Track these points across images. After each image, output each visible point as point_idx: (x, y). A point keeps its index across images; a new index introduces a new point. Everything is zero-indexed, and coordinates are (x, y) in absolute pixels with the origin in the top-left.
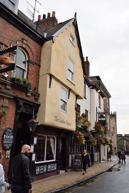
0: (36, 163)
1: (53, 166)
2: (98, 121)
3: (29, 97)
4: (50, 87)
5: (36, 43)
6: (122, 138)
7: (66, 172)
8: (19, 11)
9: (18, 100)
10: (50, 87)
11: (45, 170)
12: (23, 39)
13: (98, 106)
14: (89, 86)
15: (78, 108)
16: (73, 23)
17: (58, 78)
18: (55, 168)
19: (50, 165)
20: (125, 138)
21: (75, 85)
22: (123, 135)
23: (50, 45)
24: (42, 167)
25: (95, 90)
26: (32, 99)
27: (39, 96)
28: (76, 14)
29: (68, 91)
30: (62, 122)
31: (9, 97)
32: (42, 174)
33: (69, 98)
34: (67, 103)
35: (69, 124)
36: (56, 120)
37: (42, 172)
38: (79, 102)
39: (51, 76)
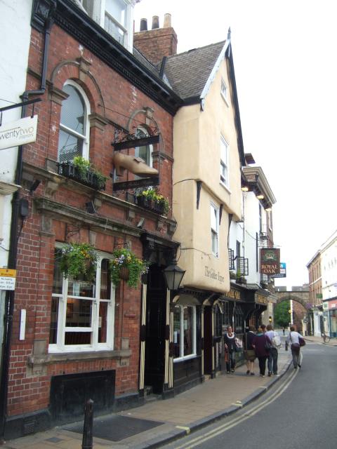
3: (131, 220)
4: (197, 208)
5: (165, 112)
6: (285, 295)
7: (212, 378)
9: (148, 239)
10: (197, 208)
12: (146, 109)
20: (292, 294)
21: (229, 193)
22: (289, 289)
25: (252, 194)
26: (164, 233)
28: (229, 31)
29: (219, 207)
30: (214, 276)
31: (74, 216)
35: (222, 279)
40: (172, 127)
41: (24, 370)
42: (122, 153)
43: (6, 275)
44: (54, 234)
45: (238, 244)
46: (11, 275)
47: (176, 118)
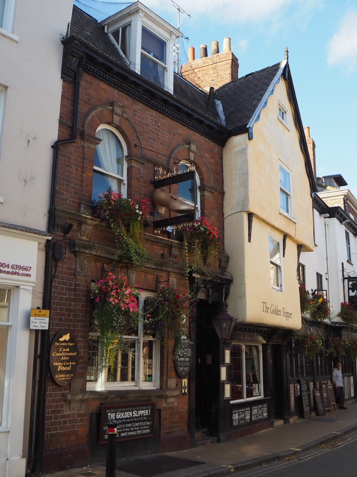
0: (231, 402)
1: (260, 408)
2: (347, 301)
4: (249, 240)
5: (212, 144)
8: (179, 80)
10: (249, 240)
11: (248, 417)
13: (345, 258)
14: (321, 213)
15: (301, 268)
16: (283, 75)
17: (263, 216)
18: (265, 414)
19: (256, 407)
21: (295, 223)
23: (244, 147)
24: (243, 412)
27: (228, 262)
30: (276, 312)
32: (243, 426)
33: (284, 256)
34: (282, 268)
35: (288, 315)
36: (264, 311)
37: (243, 422)
38: (305, 258)
39: (251, 215)
40: (221, 159)
41: (62, 406)
42: (163, 191)
43: (39, 315)
44: (90, 274)
45: (319, 276)
46: (44, 316)
47: (224, 149)
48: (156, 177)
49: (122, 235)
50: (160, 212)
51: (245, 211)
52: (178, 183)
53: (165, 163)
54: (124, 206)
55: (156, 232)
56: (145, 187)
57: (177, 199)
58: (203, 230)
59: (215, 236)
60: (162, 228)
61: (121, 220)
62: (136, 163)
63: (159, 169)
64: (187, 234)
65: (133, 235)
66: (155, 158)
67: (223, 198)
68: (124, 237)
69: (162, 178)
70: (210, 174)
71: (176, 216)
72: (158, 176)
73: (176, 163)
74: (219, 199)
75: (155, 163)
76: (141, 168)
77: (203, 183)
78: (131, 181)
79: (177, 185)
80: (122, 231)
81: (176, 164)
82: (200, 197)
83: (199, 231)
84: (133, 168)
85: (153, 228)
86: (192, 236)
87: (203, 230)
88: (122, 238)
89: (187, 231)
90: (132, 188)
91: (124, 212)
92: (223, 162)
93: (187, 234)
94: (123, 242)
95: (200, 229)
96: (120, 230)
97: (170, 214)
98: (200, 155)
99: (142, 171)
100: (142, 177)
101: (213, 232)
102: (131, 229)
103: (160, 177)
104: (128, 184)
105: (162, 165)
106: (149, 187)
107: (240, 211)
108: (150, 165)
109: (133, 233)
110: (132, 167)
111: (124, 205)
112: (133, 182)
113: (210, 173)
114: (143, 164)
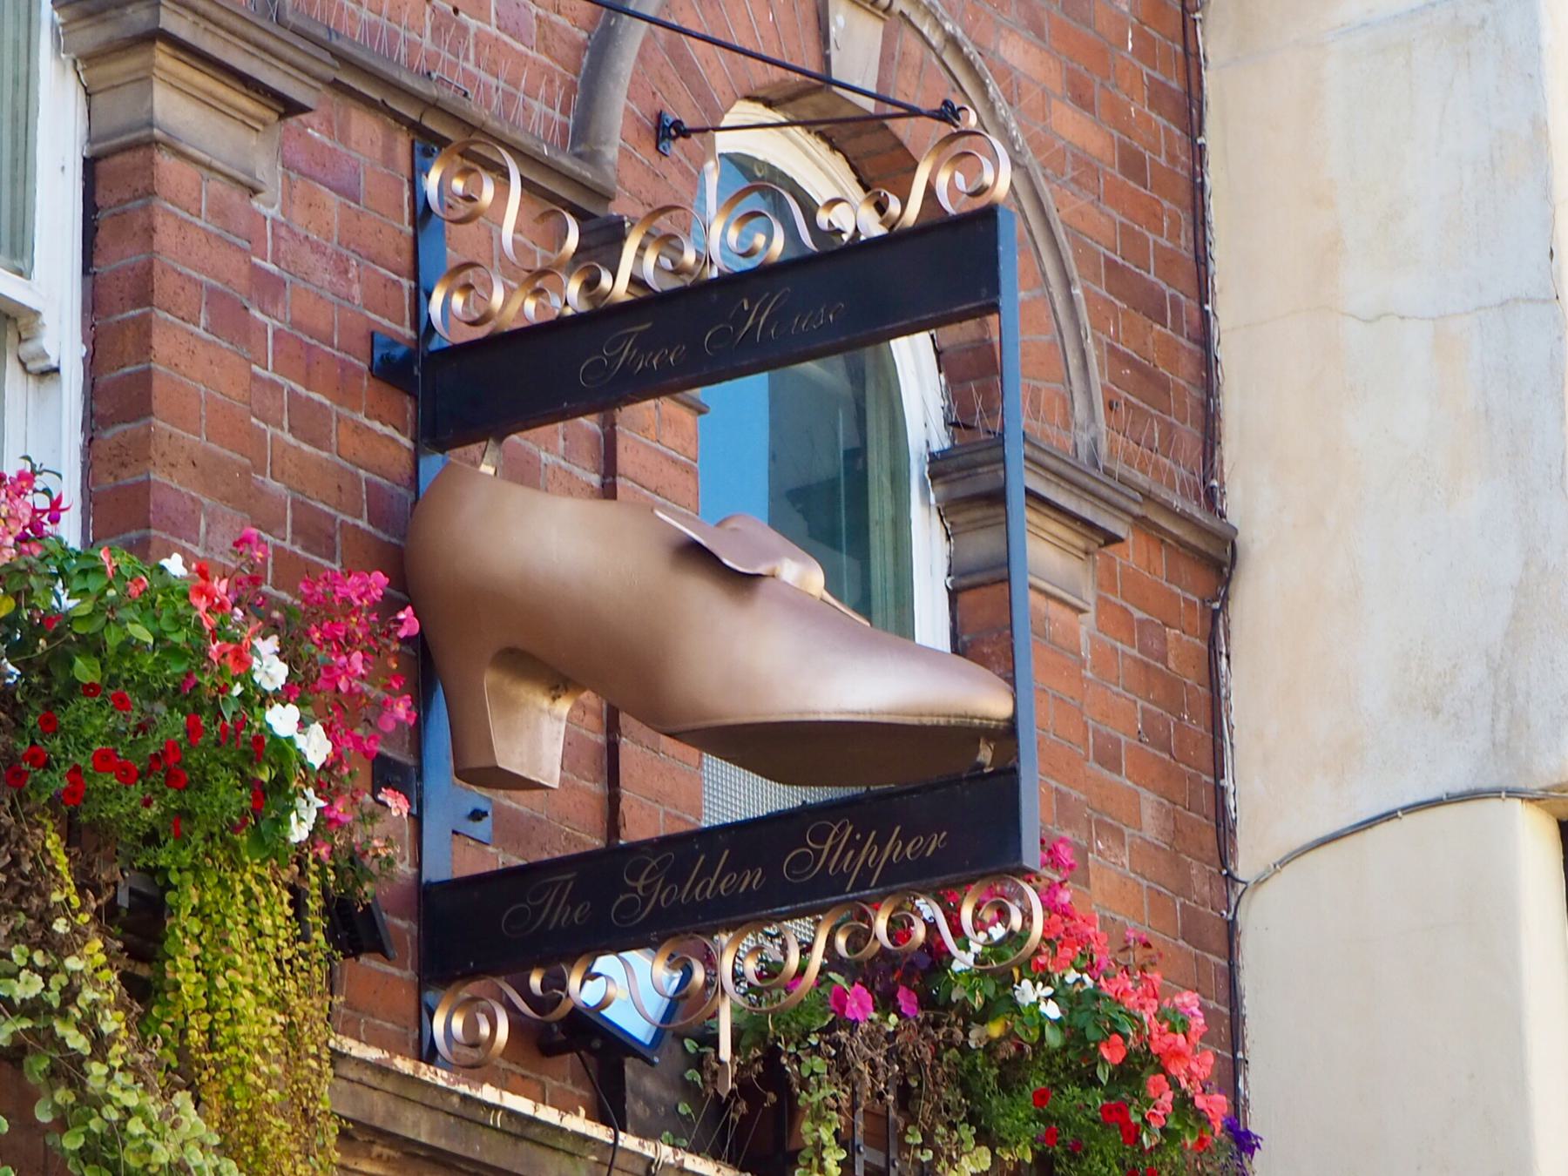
48: (438, 296)
49: (78, 1042)
50: (511, 758)
51: (1535, 784)
52: (699, 393)
53: (549, 120)
54: (113, 638)
55: (458, 1024)
56: (308, 423)
57: (767, 582)
58: (1052, 1011)
59: (1200, 1102)
60: (535, 981)
61: (71, 836)
62: (207, 101)
63: (488, 193)
64: (842, 1067)
65: (211, 1046)
66: (427, 41)
67: (1215, 614)
68: (97, 1069)
69: (530, 305)
70: (1070, 298)
71: (681, 828)
72: (467, 288)
73: (681, 131)
74: (1172, 633)
75: (433, 106)
76: (266, 169)
77: (990, 411)
78: (144, 329)
79: (686, 416)
80: (70, 994)
81: (676, 148)
82: (953, 595)
83: (995, 1030)
84: (164, 160)
85: (409, 974)
86: (906, 1096)
87: (1052, 1011)
88: (63, 1096)
89: (853, 1025)
90: (157, 422)
91: (114, 735)
92: (1202, 148)
93: (842, 1067)
94: (72, 1142)
95: (1015, 1006)
96: (46, 973)
97: (614, 800)
98: (952, 40)
99: (268, 208)
100: (268, 287)
101: (1179, 1054)
102: (184, 973)
103: (498, 298)
104: (92, 364)
105: (525, 157)
106: (358, 429)
107: (1461, 786)
108: (365, 129)
109: (211, 1032)
110: (151, 144)
111: (120, 623)
112: (162, 344)
113: (1068, 283)
114: (289, 108)
